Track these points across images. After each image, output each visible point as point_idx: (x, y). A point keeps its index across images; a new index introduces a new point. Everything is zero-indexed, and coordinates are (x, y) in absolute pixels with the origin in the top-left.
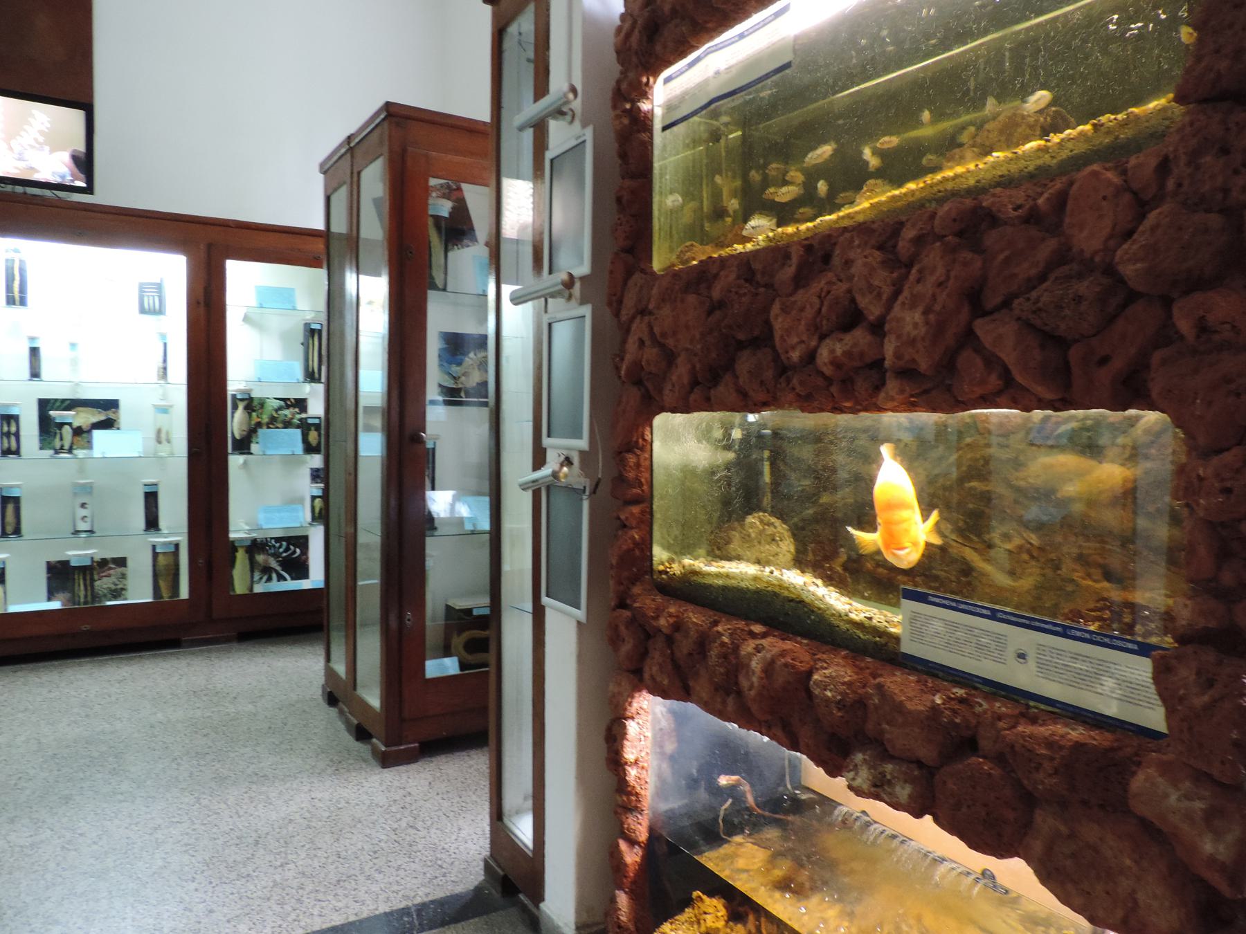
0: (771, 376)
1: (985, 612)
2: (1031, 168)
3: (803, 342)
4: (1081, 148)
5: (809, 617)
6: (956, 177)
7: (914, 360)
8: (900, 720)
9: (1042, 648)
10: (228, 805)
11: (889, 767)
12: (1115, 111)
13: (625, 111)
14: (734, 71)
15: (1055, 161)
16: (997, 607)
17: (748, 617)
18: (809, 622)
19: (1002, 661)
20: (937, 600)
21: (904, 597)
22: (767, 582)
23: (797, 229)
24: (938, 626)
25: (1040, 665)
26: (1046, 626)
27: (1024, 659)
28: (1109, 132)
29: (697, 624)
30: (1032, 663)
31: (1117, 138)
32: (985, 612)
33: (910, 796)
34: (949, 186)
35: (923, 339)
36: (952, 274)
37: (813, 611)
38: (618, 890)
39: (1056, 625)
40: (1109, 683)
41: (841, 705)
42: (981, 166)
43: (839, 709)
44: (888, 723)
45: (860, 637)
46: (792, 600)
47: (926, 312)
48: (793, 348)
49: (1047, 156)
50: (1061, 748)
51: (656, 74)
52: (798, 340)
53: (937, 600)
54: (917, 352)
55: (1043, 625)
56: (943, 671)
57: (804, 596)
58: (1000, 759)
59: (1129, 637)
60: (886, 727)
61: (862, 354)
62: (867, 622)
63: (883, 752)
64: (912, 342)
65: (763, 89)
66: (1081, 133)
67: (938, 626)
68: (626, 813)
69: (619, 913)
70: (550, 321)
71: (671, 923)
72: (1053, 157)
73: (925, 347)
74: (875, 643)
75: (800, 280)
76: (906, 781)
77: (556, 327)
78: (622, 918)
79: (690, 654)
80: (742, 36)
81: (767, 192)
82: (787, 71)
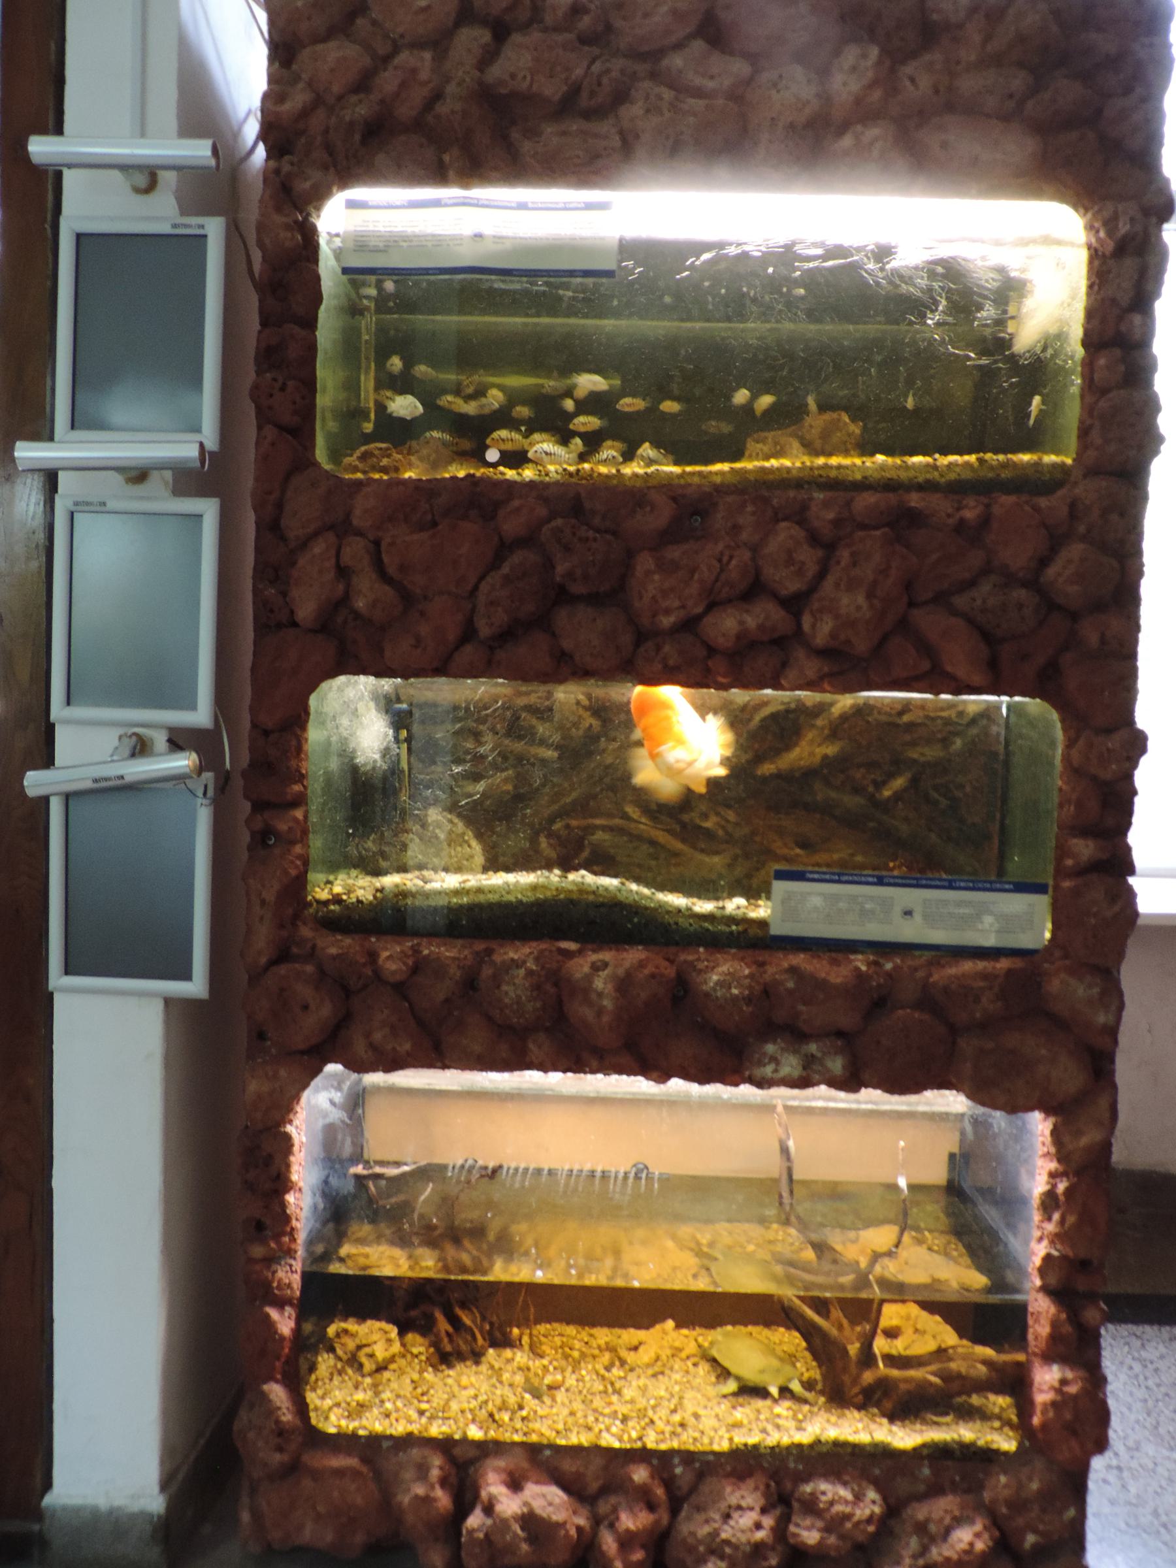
2: (920, 479)
4: (967, 475)
5: (631, 921)
6: (839, 467)
8: (821, 996)
10: (448, 1401)
11: (813, 1048)
12: (996, 453)
13: (296, 222)
14: (508, 245)
15: (943, 480)
17: (559, 933)
20: (816, 876)
22: (557, 889)
23: (618, 471)
24: (817, 901)
25: (926, 917)
28: (992, 468)
29: (454, 959)
30: (918, 917)
31: (998, 475)
33: (844, 1067)
34: (833, 474)
38: (265, 1383)
40: (988, 920)
41: (749, 1000)
42: (868, 464)
43: (747, 1005)
44: (805, 1004)
46: (602, 905)
48: (667, 612)
49: (936, 473)
50: (996, 977)
51: (344, 183)
53: (816, 876)
58: (919, 1005)
60: (801, 1008)
63: (796, 1035)
65: (566, 287)
66: (967, 464)
67: (817, 901)
68: (269, 1267)
69: (279, 1413)
70: (73, 508)
71: (314, 1389)
72: (942, 476)
74: (731, 933)
75: (673, 534)
76: (836, 1054)
77: (75, 515)
78: (284, 1419)
79: (447, 1000)
80: (522, 206)
81: (443, 398)
82: (604, 280)
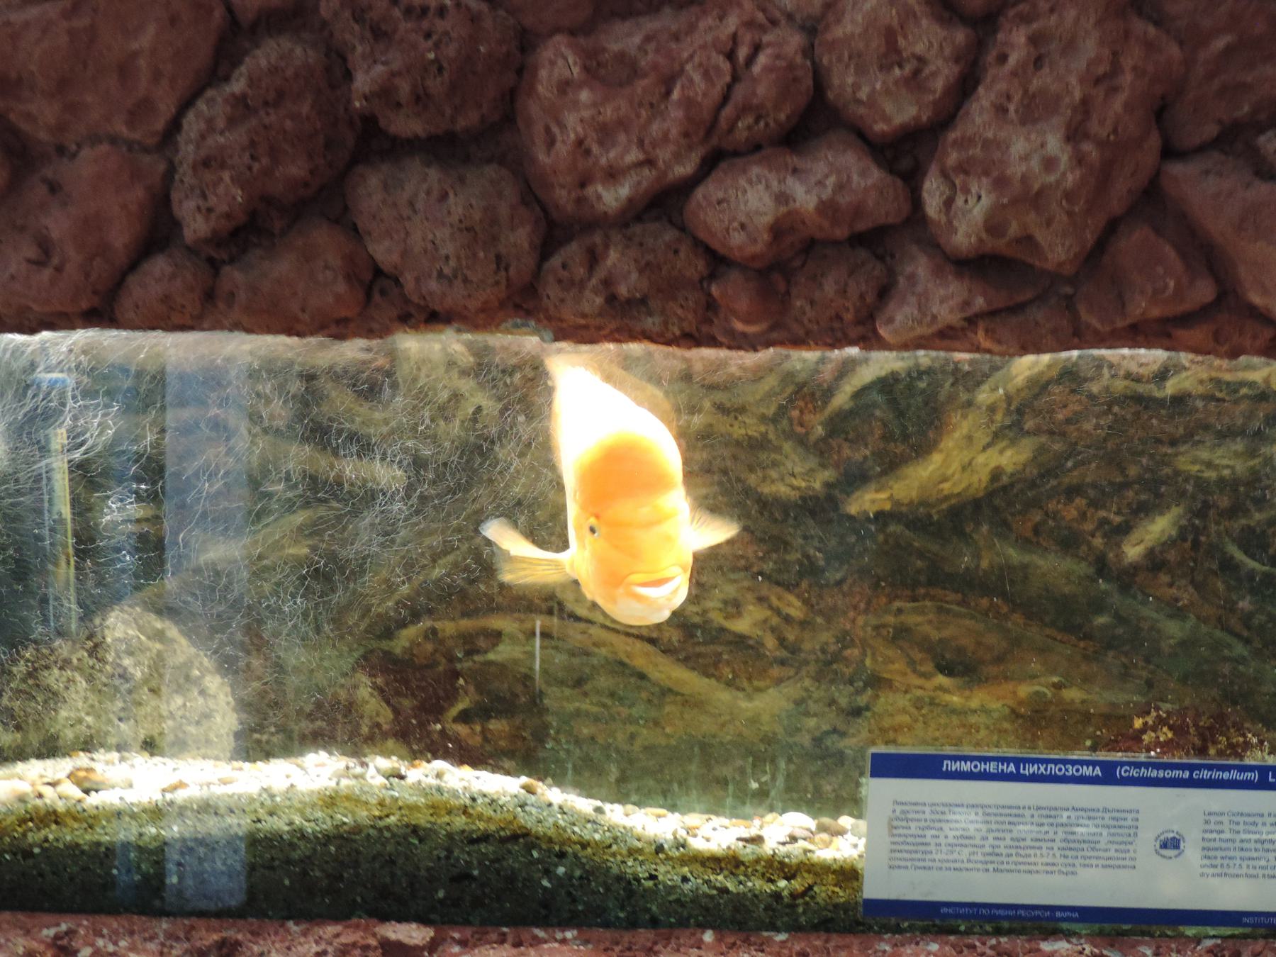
0: (526, 245)
1: (1087, 771)
3: (650, 162)
5: (547, 872)
7: (1027, 240)
9: (1213, 819)
16: (1118, 756)
18: (545, 883)
19: (1127, 863)
21: (874, 774)
22: (381, 804)
24: (967, 822)
26: (1226, 776)
27: (1177, 847)
30: (1192, 852)
32: (1087, 771)
35: (1069, 196)
36: (1127, 62)
37: (562, 855)
39: (1243, 769)
45: (724, 891)
46: (485, 838)
47: (1073, 135)
48: (613, 175)
52: (641, 157)
54: (1049, 223)
55: (982, 767)
56: (965, 917)
57: (527, 820)
59: (1231, 762)
61: (858, 211)
62: (748, 852)
64: (1034, 199)
67: (967, 822)
73: (1070, 214)
74: (777, 896)
